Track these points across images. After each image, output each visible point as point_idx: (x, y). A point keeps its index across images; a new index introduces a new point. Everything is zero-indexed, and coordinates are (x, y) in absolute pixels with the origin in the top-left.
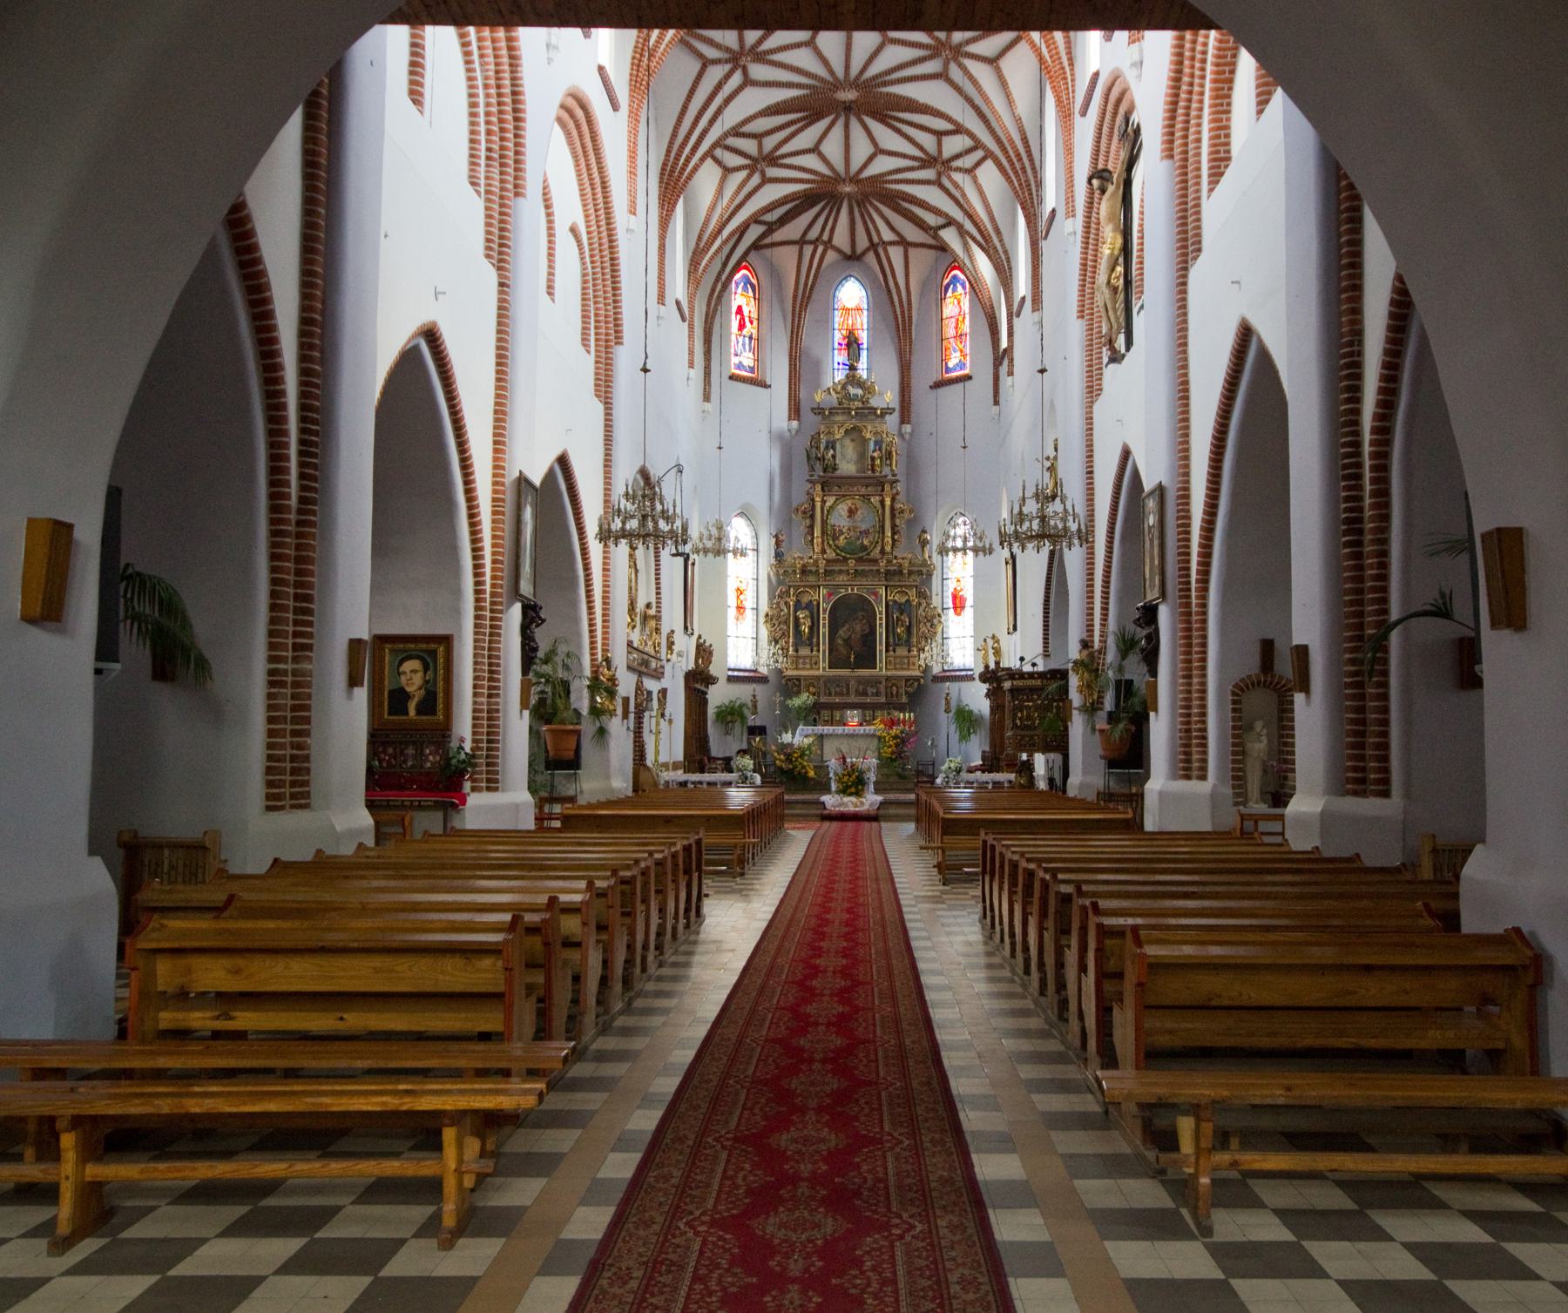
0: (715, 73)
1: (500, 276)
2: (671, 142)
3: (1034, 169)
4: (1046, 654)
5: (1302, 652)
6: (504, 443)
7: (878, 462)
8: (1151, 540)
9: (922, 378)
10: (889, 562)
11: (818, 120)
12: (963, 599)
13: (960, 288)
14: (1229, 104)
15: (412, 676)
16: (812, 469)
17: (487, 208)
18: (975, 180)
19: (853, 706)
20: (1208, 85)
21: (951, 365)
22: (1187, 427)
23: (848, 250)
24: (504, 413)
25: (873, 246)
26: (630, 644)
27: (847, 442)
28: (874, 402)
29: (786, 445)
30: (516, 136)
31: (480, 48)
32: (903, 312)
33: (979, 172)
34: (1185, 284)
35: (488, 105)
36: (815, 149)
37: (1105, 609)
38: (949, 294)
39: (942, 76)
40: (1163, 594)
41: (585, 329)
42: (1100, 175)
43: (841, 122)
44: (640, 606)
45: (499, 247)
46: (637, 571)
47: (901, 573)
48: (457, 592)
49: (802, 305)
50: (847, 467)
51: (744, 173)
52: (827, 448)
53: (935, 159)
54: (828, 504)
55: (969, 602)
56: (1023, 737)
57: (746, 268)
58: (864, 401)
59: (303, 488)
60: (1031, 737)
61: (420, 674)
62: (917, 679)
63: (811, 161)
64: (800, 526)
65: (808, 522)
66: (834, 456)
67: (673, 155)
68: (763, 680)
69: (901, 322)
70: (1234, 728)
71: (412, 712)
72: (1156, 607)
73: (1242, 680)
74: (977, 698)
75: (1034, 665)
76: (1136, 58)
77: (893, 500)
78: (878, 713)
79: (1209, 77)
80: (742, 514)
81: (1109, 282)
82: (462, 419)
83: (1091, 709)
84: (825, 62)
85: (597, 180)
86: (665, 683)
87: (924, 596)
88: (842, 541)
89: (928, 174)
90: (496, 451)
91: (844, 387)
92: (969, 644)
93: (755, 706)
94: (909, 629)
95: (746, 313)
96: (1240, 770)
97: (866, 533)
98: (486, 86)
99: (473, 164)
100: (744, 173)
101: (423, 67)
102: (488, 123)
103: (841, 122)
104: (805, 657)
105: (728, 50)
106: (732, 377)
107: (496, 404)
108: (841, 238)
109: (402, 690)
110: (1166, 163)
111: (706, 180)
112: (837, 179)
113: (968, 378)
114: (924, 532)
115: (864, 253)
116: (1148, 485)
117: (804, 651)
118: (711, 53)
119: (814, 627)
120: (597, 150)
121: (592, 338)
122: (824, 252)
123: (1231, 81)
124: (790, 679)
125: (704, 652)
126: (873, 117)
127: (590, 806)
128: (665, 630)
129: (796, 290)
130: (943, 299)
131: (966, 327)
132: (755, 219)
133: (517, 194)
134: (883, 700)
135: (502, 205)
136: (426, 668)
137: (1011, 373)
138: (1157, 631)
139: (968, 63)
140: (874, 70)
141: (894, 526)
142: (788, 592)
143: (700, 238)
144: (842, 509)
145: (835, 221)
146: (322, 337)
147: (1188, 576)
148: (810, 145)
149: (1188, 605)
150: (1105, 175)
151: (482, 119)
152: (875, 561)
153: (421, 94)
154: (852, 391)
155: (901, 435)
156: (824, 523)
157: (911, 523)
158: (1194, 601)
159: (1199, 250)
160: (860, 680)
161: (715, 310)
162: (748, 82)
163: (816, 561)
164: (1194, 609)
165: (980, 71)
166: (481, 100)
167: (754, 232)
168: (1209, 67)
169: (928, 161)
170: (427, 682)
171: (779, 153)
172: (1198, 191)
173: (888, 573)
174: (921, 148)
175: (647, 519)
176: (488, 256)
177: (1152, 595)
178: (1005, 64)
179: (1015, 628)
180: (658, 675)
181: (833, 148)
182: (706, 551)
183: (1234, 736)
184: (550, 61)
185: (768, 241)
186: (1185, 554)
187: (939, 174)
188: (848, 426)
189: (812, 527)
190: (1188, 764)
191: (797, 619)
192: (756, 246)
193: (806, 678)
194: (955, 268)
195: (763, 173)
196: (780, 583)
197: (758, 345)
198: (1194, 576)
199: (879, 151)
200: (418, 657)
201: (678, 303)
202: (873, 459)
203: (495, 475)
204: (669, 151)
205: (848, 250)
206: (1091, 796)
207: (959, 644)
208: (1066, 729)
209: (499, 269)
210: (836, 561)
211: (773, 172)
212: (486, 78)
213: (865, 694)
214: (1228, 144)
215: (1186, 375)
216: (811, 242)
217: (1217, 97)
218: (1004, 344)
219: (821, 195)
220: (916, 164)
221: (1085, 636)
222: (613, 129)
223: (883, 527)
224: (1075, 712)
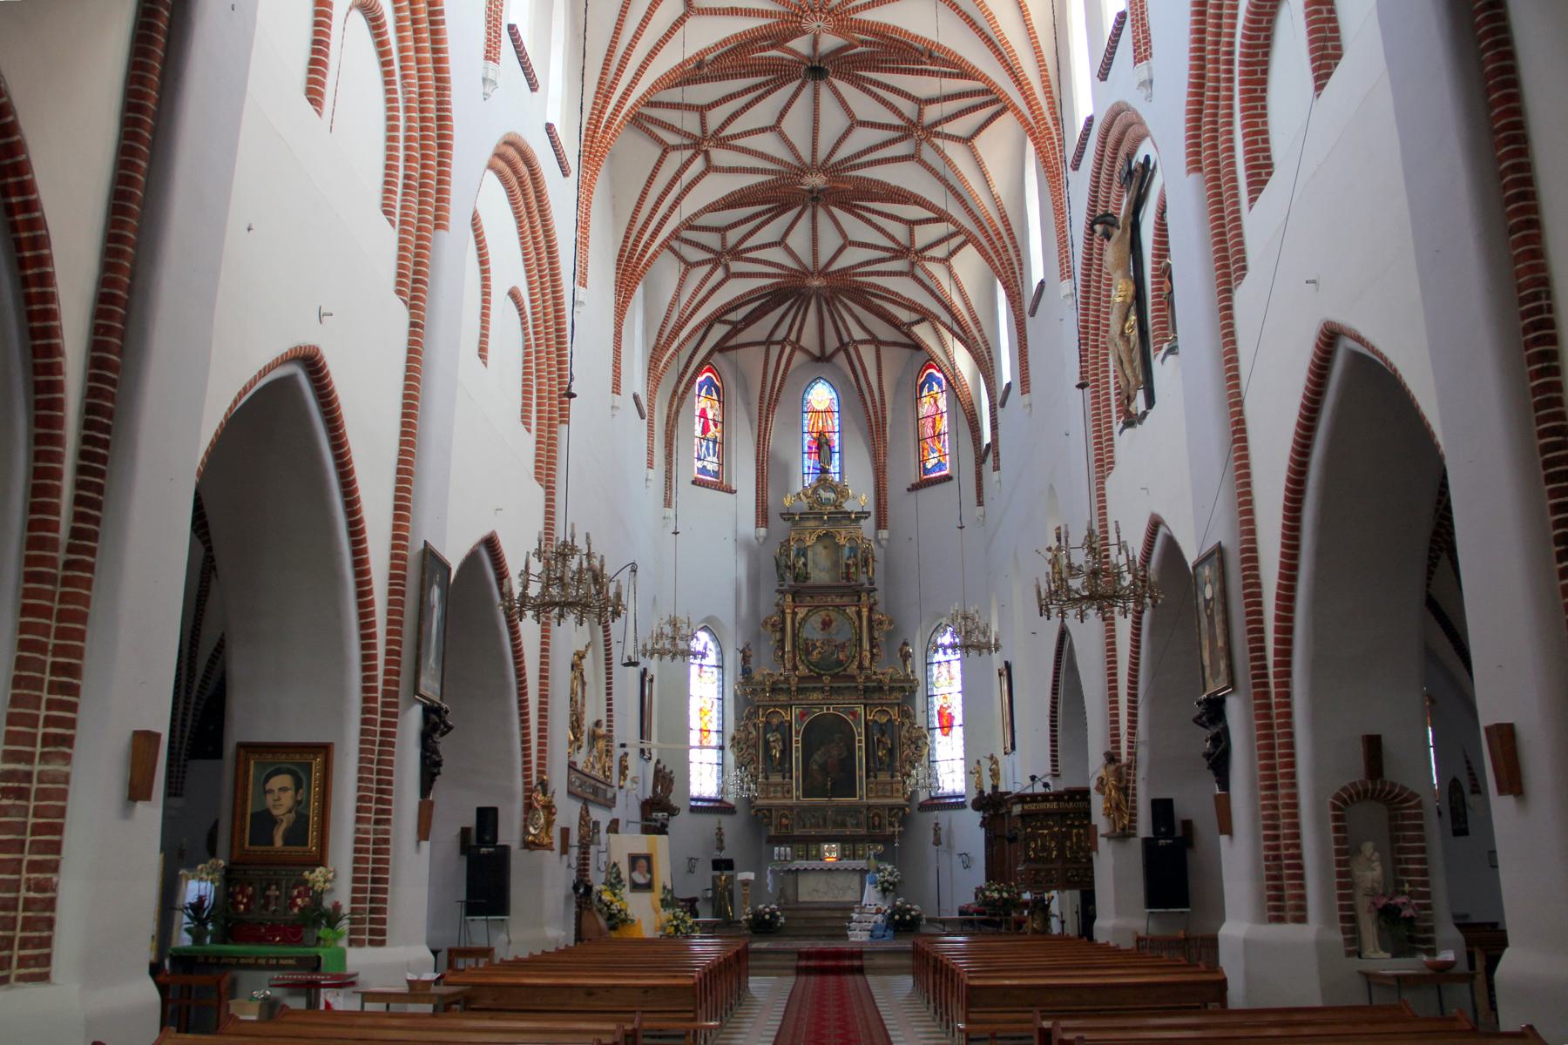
0: (675, 160)
1: (412, 315)
2: (629, 229)
3: (1015, 247)
4: (1055, 774)
5: (1505, 736)
6: (407, 509)
7: (853, 570)
8: (1211, 618)
9: (902, 474)
10: (868, 678)
11: (783, 212)
12: (951, 717)
13: (936, 387)
14: (1264, 107)
15: (281, 796)
16: (782, 578)
17: (401, 240)
19: (829, 840)
20: (1237, 87)
21: (929, 466)
22: (1248, 475)
23: (816, 352)
24: (410, 473)
25: (843, 346)
26: (572, 766)
28: (848, 506)
29: (752, 552)
30: (440, 164)
31: (402, 68)
32: (876, 413)
33: (955, 262)
34: (1230, 308)
35: (409, 129)
36: (781, 243)
37: (1133, 715)
38: (925, 393)
40: (1232, 683)
41: (526, 407)
42: (1101, 221)
43: (807, 215)
44: (588, 722)
45: (414, 281)
46: (584, 684)
47: (881, 689)
48: (341, 691)
49: (771, 402)
51: (707, 268)
52: (797, 556)
53: (908, 249)
54: (800, 616)
55: (958, 720)
56: (1038, 871)
57: (709, 370)
58: (837, 505)
59: (78, 517)
60: (1049, 871)
61: (290, 793)
62: (902, 808)
63: (776, 255)
65: (778, 636)
66: (805, 565)
67: (631, 241)
69: (871, 419)
70: (1338, 852)
71: (278, 842)
72: (1222, 700)
73: (1344, 789)
74: (969, 831)
75: (1046, 785)
76: (1145, 76)
77: (871, 610)
79: (1237, 79)
80: (704, 629)
81: (1122, 333)
82: (351, 472)
83: (1123, 834)
84: (791, 147)
85: (543, 244)
86: (617, 812)
87: (907, 714)
90: (397, 517)
91: (815, 491)
92: (960, 767)
94: (891, 752)
95: (710, 416)
96: (1351, 908)
97: (843, 646)
98: (408, 109)
99: (387, 191)
100: (707, 268)
101: (325, 65)
102: (407, 148)
103: (807, 215)
104: (776, 785)
105: (687, 135)
106: (695, 482)
107: (400, 462)
108: (809, 339)
109: (267, 812)
110: (1194, 176)
111: (666, 273)
112: (805, 273)
113: (948, 478)
114: (906, 644)
115: (834, 354)
116: (1191, 556)
117: (776, 778)
118: (672, 139)
119: (786, 751)
120: (543, 211)
121: (534, 415)
123: (1264, 82)
124: (759, 810)
126: (841, 208)
127: (518, 964)
128: (618, 752)
129: (763, 392)
130: (918, 399)
131: (943, 425)
132: (717, 317)
133: (437, 227)
134: (863, 831)
135: (419, 238)
136: (298, 785)
137: (996, 468)
138: (1226, 730)
139: (938, 142)
141: (872, 639)
142: (756, 712)
143: (660, 334)
144: (816, 620)
145: (803, 319)
146: (124, 321)
147: (1264, 658)
148: (776, 238)
149: (1266, 695)
150: (1110, 219)
151: (401, 144)
152: (852, 678)
153: (321, 94)
154: (824, 495)
155: (878, 541)
156: (795, 636)
157: (890, 635)
158: (1273, 689)
159: (1244, 268)
160: (840, 810)
162: (710, 168)
163: (787, 679)
164: (1274, 700)
165: (954, 151)
166: (402, 123)
167: (719, 331)
168: (1237, 68)
169: (901, 252)
170: (298, 803)
171: (729, 131)
172: (1236, 203)
173: (866, 690)
174: (893, 239)
175: (580, 589)
176: (399, 292)
177: (1214, 687)
178: (980, 143)
179: (1013, 747)
180: (609, 804)
181: (799, 240)
182: (662, 653)
183: (1339, 864)
184: (486, 97)
185: (732, 342)
186: (1256, 631)
187: (913, 264)
188: (821, 532)
189: (782, 641)
190: (1281, 902)
191: (767, 742)
192: (720, 347)
193: (778, 808)
194: (931, 367)
195: (727, 267)
197: (722, 448)
198: (1271, 659)
199: (848, 243)
200: (289, 772)
201: (636, 397)
202: (848, 566)
203: (394, 547)
204: (627, 237)
205: (816, 352)
206: (1128, 944)
207: (949, 766)
208: (1090, 860)
209: (412, 307)
210: (809, 678)
211: (736, 266)
212: (409, 100)
213: (843, 825)
214: (1267, 150)
215: (1241, 413)
216: (778, 343)
217: (1249, 100)
218: (987, 438)
219: (788, 292)
220: (887, 255)
221: (1109, 748)
222: (561, 193)
223: (860, 640)
224: (1102, 842)
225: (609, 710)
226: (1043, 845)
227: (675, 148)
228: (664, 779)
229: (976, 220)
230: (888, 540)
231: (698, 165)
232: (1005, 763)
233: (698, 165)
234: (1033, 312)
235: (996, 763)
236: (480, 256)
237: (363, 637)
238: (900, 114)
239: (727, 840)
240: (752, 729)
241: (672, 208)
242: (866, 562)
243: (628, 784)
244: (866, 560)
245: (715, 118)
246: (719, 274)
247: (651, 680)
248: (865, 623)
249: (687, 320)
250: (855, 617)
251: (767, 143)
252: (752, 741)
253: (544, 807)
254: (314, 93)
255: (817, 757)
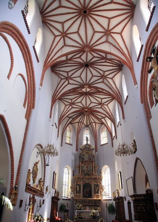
9: (98, 146)
16: (80, 159)
18: (108, 107)
19: (87, 206)
23: (86, 124)
25: (90, 123)
27: (86, 155)
29: (75, 156)
36: (81, 102)
39: (103, 82)
50: (86, 159)
51: (68, 106)
54: (83, 166)
58: (89, 148)
64: (78, 169)
66: (84, 157)
68: (69, 200)
78: (92, 207)
84: (82, 80)
88: (85, 172)
89: (100, 106)
93: (68, 205)
97: (89, 171)
103: (85, 97)
105: (64, 76)
108: (85, 122)
114: (100, 170)
117: (78, 194)
118: (63, 77)
122: (82, 124)
125: (57, 193)
134: (93, 204)
139: (107, 79)
140: (90, 83)
141: (95, 170)
143: (61, 116)
144: (85, 166)
145: (84, 119)
156: (82, 169)
161: (64, 131)
162: (69, 83)
171: (72, 76)
187: (102, 106)
189: (80, 170)
191: (76, 187)
192: (71, 123)
195: (72, 106)
196: (74, 180)
204: (54, 93)
205: (86, 124)
209: (27, 120)
213: (90, 203)
220: (97, 104)
223: (93, 170)
225: (44, 177)
226: (141, 208)
227: (63, 79)
228: (57, 193)
229: (114, 92)
230: (97, 154)
231: (67, 82)
232: (120, 192)
233: (67, 82)
234: (125, 104)
235: (118, 191)
236: (11, 58)
237: (12, 169)
238: (101, 74)
239: (69, 205)
240: (74, 185)
241: (62, 89)
242: (94, 157)
243: (47, 193)
244: (94, 156)
245: (70, 74)
246: (71, 107)
247: (56, 174)
248: (94, 167)
249: (65, 115)
250: (92, 166)
251: (78, 79)
252: (75, 188)
253: (14, 194)
254: (8, 77)
255: (85, 190)
